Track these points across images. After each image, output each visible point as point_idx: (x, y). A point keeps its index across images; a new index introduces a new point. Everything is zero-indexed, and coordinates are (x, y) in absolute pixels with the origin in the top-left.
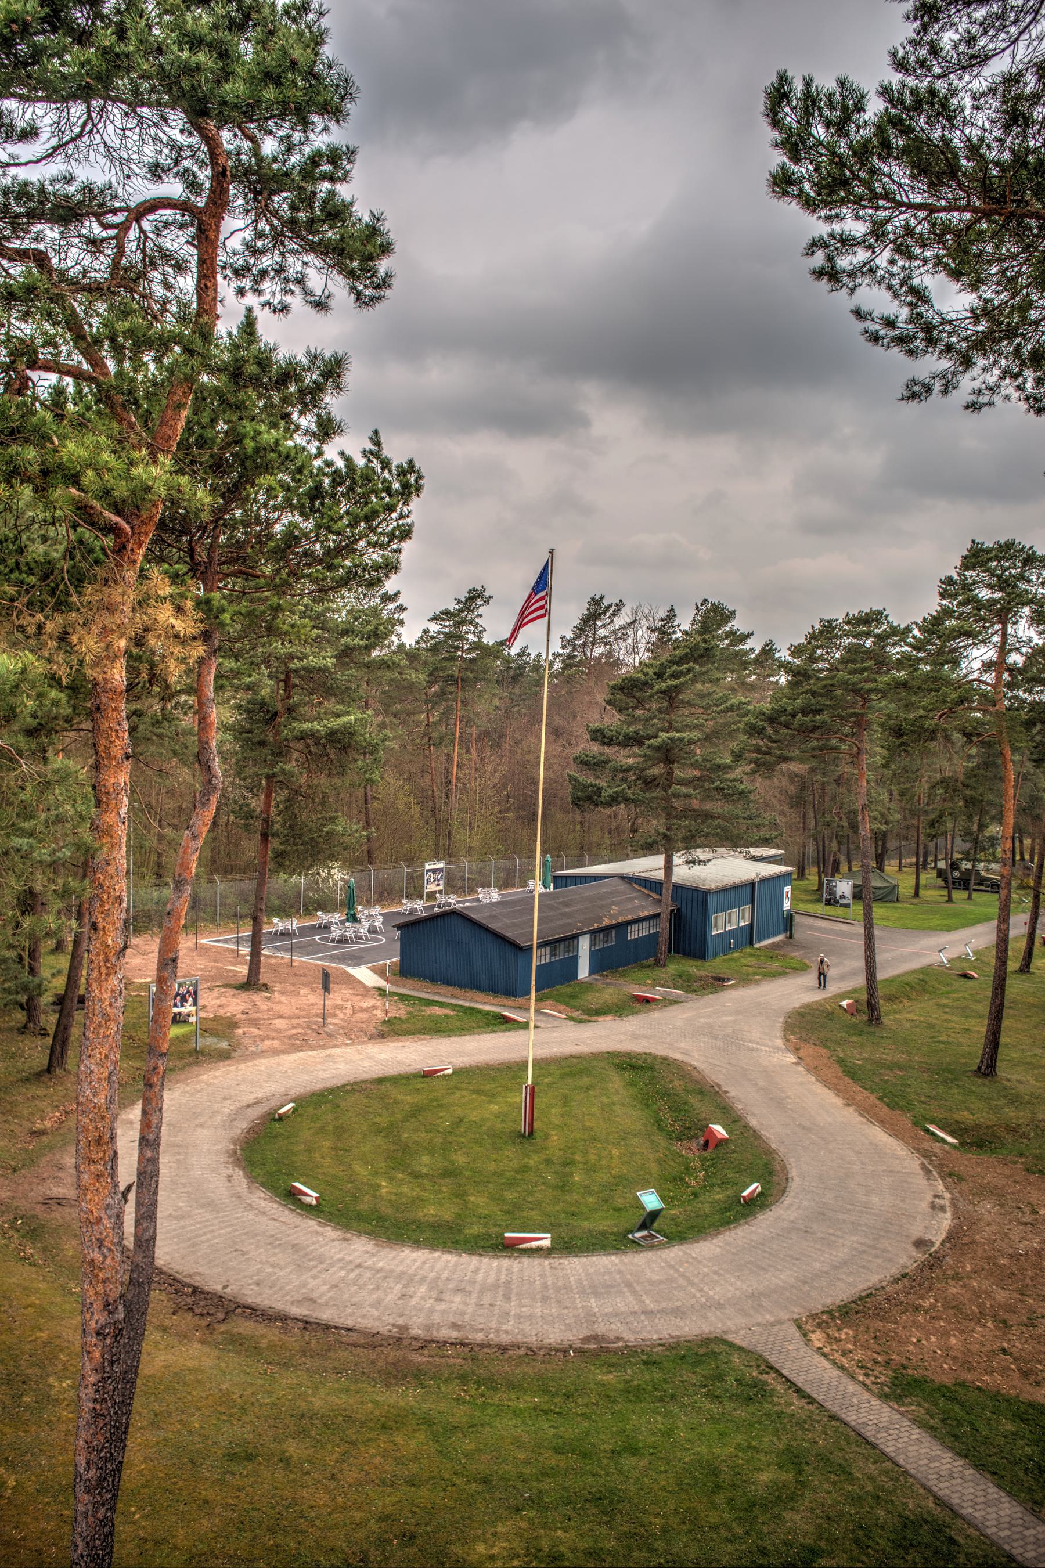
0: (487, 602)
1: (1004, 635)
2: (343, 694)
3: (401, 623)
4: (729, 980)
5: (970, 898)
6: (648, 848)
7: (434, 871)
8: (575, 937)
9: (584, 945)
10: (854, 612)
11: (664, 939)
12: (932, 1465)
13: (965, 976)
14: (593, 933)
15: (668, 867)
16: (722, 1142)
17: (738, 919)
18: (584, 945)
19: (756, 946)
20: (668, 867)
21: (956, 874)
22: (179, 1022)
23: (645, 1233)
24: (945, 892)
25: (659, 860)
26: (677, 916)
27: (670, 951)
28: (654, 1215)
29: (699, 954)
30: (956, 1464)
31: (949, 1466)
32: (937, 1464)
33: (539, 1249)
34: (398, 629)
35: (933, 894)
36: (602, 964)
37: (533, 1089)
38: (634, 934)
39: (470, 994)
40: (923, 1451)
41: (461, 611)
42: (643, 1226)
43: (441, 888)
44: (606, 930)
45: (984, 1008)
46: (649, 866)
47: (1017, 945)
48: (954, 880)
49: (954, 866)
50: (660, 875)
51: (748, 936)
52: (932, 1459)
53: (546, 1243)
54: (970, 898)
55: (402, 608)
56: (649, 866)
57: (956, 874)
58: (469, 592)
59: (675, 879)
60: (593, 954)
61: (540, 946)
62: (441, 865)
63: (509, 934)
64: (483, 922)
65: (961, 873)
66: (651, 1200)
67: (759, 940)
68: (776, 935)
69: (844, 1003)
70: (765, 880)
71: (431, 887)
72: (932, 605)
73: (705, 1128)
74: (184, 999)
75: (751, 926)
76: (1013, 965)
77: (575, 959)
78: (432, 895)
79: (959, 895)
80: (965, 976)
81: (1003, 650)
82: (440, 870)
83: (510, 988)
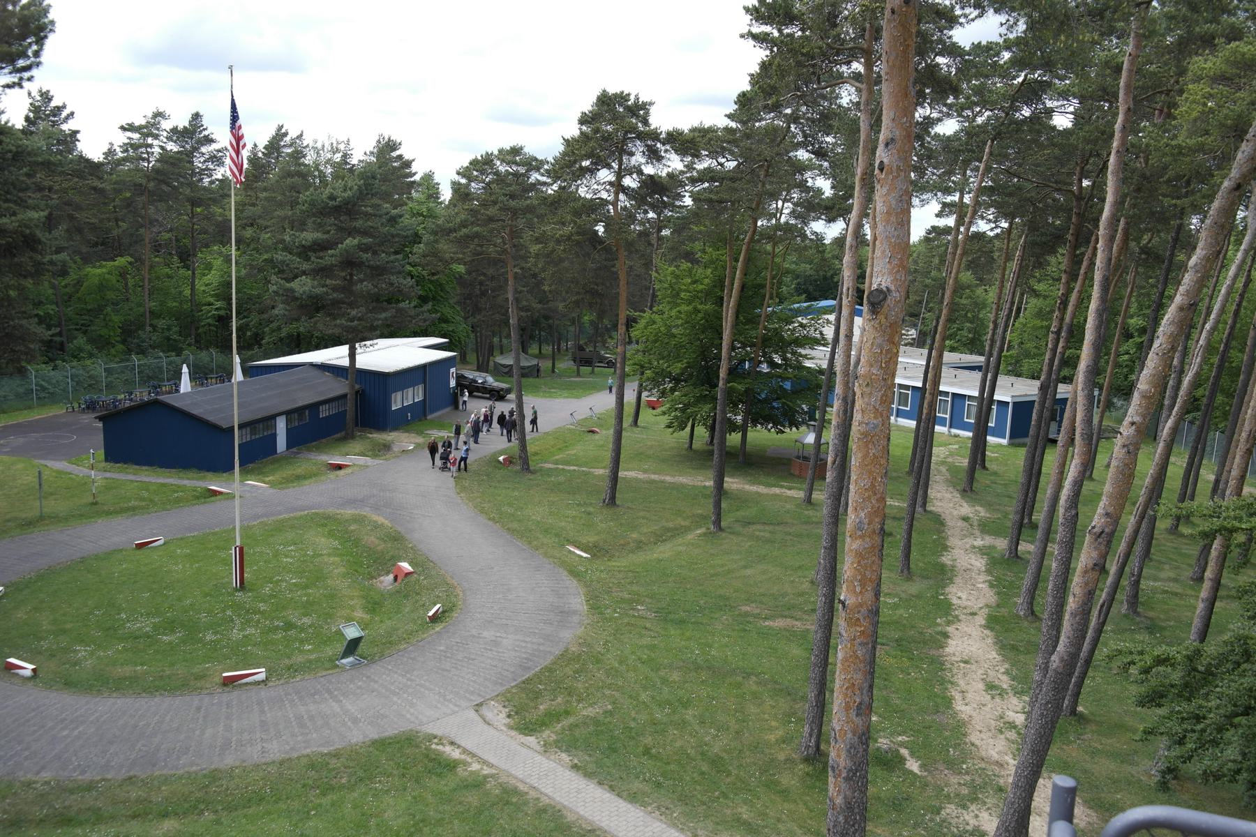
5: (593, 372)
6: (336, 342)
8: (273, 418)
9: (281, 425)
11: (350, 416)
13: (593, 432)
14: (288, 413)
15: (352, 355)
16: (408, 574)
17: (414, 395)
18: (281, 425)
20: (352, 355)
23: (351, 659)
25: (344, 350)
26: (360, 395)
29: (382, 426)
33: (258, 683)
35: (565, 364)
36: (295, 440)
38: (324, 412)
39: (191, 474)
42: (346, 654)
44: (300, 410)
45: (608, 455)
46: (337, 355)
47: (629, 410)
50: (345, 362)
53: (262, 676)
54: (593, 372)
59: (358, 366)
60: (289, 432)
61: (241, 427)
63: (211, 418)
66: (352, 632)
69: (501, 458)
75: (424, 400)
76: (628, 421)
77: (274, 436)
79: (585, 370)
80: (593, 432)
83: (222, 466)
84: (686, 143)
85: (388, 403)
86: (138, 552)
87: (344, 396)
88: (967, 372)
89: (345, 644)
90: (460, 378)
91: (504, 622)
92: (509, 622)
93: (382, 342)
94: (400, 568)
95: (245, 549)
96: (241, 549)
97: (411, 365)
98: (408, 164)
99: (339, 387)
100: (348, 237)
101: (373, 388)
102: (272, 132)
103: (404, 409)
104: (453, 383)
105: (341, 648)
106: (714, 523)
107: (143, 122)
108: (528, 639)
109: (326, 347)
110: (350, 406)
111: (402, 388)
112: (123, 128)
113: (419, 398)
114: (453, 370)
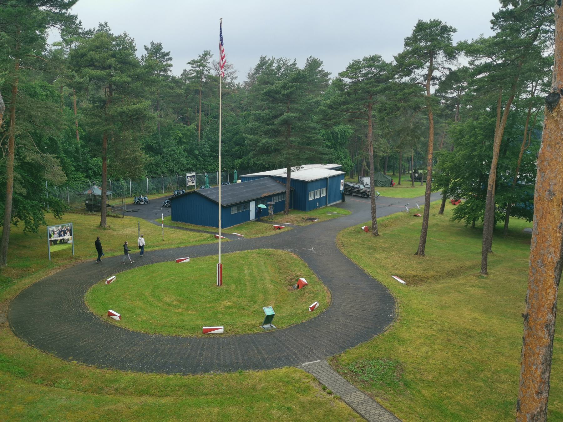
0: (212, 56)
1: (431, 63)
2: (138, 95)
3: (171, 65)
4: (315, 219)
6: (280, 167)
7: (191, 177)
10: (368, 56)
11: (287, 202)
12: (380, 418)
13: (416, 216)
19: (328, 205)
20: (289, 172)
21: (416, 175)
22: (63, 243)
24: (411, 183)
25: (285, 170)
27: (290, 207)
28: (272, 317)
30: (390, 417)
31: (388, 418)
32: (382, 417)
34: (171, 68)
37: (221, 265)
40: (377, 412)
41: (201, 60)
43: (194, 184)
46: (281, 172)
48: (415, 178)
49: (416, 172)
50: (285, 176)
51: (324, 201)
52: (380, 416)
55: (171, 59)
56: (281, 172)
57: (416, 175)
58: (205, 51)
62: (194, 174)
64: (207, 196)
65: (419, 174)
66: (269, 311)
67: (330, 203)
68: (338, 200)
69: (363, 228)
70: (332, 177)
71: (190, 184)
72: (401, 49)
73: (298, 280)
74: (65, 233)
75: (326, 196)
77: (249, 211)
78: (190, 187)
80: (416, 216)
81: (431, 69)
82: (193, 176)
84: (471, 49)
85: (306, 197)
86: (177, 264)
87: (284, 193)
88: (219, 34)
89: (265, 317)
90: (345, 185)
91: (351, 314)
92: (354, 315)
93: (306, 167)
94: (301, 281)
95: (223, 266)
96: (221, 265)
97: (320, 177)
98: (327, 74)
99: (279, 189)
100: (290, 110)
101: (300, 188)
102: (258, 61)
103: (315, 200)
104: (342, 188)
105: (263, 320)
106: (482, 269)
107: (199, 58)
108: (363, 325)
109: (276, 169)
110: (287, 198)
111: (315, 189)
112: (189, 63)
113: (324, 195)
114: (342, 181)
